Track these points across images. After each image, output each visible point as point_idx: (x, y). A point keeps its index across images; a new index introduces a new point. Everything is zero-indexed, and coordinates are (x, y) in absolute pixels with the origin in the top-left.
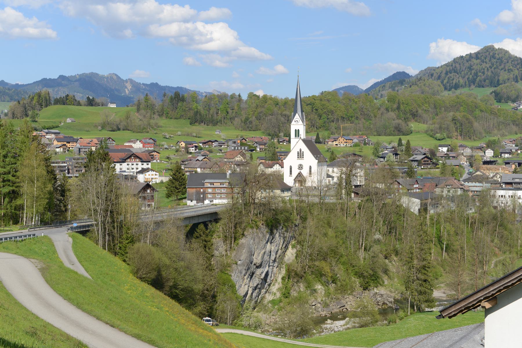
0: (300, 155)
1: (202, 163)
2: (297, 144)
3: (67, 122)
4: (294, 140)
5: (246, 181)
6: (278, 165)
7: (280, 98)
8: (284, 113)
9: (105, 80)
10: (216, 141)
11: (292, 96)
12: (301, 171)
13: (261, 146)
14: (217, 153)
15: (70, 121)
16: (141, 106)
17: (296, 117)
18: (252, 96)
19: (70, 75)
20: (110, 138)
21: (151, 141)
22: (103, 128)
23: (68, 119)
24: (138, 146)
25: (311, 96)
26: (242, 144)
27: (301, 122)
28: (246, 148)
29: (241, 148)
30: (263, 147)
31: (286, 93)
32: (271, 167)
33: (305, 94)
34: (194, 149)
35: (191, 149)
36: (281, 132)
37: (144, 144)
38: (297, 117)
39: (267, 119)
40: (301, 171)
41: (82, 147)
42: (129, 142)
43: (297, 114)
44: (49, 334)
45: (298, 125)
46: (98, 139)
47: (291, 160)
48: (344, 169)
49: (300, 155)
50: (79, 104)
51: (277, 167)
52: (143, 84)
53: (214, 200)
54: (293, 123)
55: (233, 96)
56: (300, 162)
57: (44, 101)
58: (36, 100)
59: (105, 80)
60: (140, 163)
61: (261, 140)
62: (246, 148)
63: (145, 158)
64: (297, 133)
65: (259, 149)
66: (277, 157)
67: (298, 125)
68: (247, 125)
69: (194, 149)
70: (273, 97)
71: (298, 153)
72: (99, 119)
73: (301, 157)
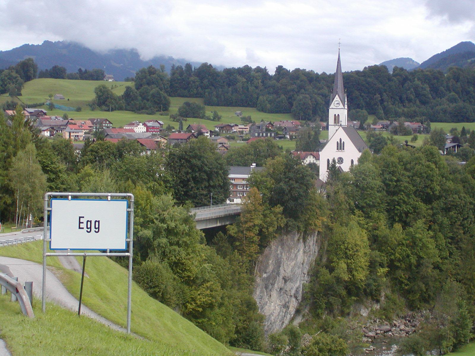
0: (340, 146)
6: (312, 157)
8: (460, 200)
11: (331, 70)
18: (280, 69)
25: (353, 70)
26: (268, 130)
27: (341, 106)
28: (273, 135)
29: (267, 135)
33: (345, 69)
34: (209, 134)
36: (320, 112)
39: (297, 95)
41: (73, 130)
43: (337, 96)
45: (338, 109)
46: (92, 120)
47: (328, 153)
49: (340, 146)
53: (235, 200)
55: (259, 69)
58: (23, 68)
62: (273, 135)
64: (337, 119)
67: (338, 109)
73: (341, 149)
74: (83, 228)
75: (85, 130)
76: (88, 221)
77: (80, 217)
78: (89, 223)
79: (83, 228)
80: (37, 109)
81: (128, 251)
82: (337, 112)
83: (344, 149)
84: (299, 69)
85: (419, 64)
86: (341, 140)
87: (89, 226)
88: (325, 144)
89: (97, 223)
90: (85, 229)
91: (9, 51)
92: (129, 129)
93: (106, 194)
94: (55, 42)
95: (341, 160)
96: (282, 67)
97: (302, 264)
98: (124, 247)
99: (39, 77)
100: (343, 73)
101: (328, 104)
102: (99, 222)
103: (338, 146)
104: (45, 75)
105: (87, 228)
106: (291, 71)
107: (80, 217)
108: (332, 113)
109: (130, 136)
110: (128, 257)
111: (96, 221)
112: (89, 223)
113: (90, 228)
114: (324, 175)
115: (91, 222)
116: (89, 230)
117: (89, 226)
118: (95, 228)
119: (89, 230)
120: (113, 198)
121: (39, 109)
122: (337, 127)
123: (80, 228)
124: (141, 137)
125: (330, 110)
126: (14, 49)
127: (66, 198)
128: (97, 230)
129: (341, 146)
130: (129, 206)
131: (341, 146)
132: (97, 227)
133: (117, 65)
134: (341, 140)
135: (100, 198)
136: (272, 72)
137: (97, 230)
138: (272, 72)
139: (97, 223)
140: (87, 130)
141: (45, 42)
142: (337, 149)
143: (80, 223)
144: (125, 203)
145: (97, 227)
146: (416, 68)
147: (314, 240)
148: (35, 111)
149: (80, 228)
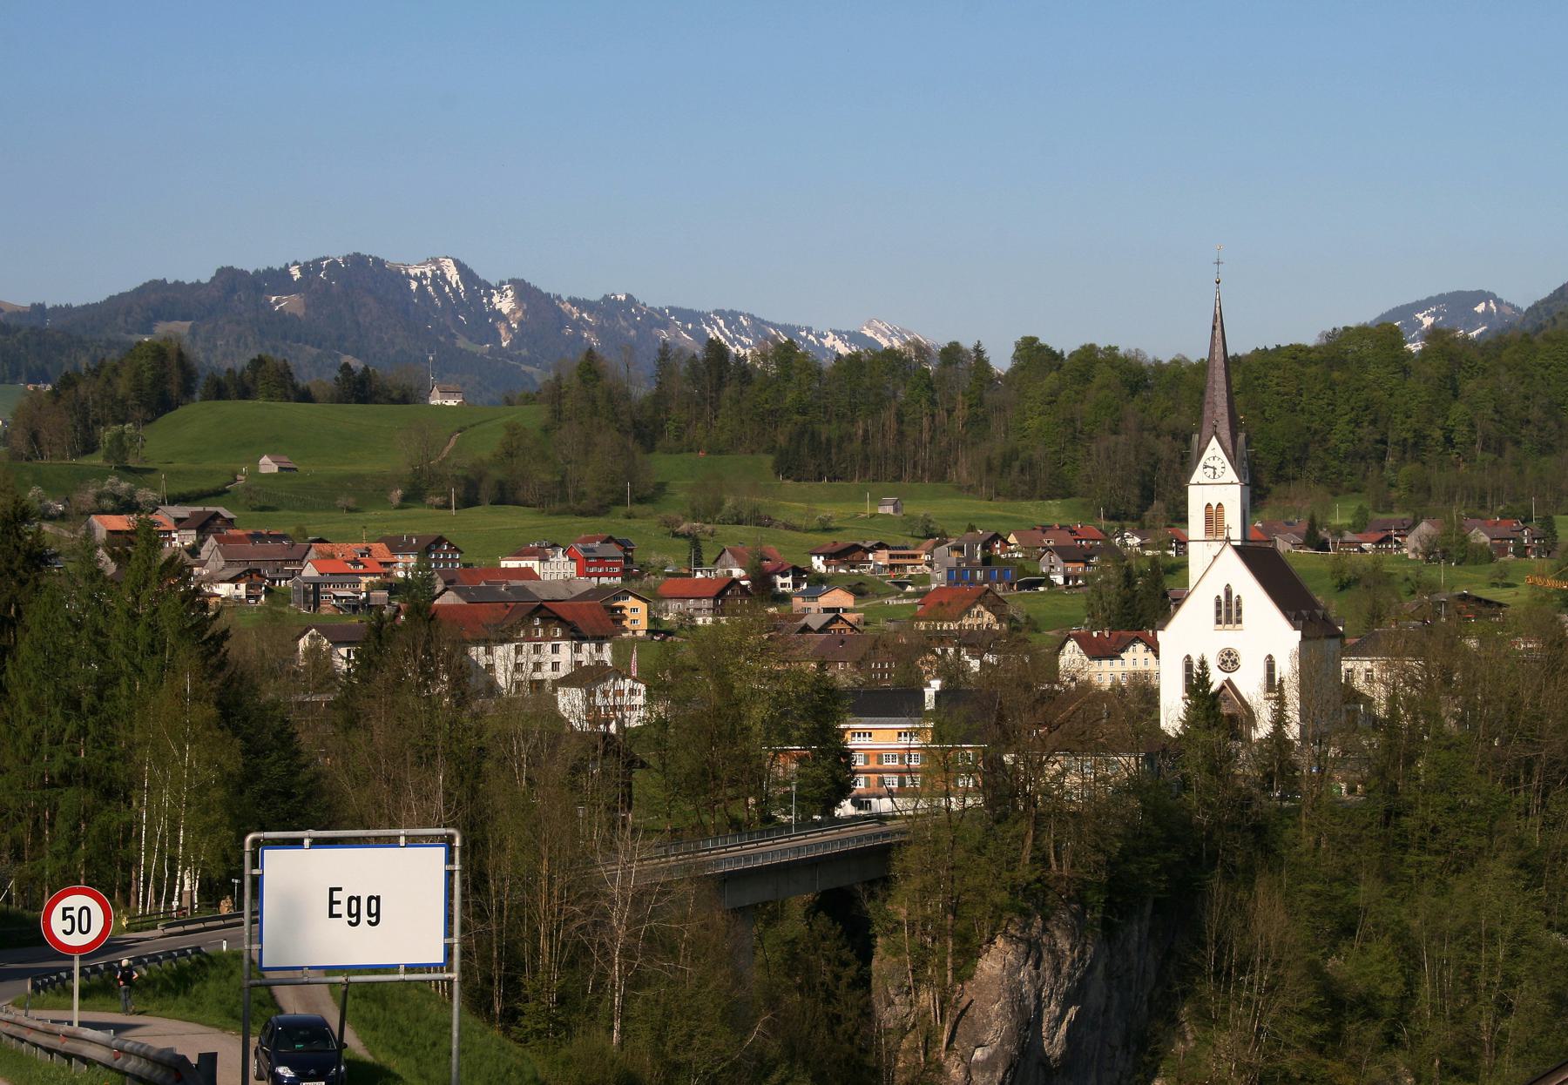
0: (1228, 611)
1: (824, 643)
2: (1215, 568)
3: (263, 470)
4: (1199, 554)
5: (1004, 714)
6: (1140, 647)
7: (1150, 358)
9: (414, 285)
10: (881, 546)
11: (1196, 349)
12: (1233, 677)
13: (1070, 567)
14: (888, 595)
15: (275, 469)
16: (567, 403)
17: (1208, 453)
18: (1032, 353)
19: (262, 267)
20: (440, 541)
21: (613, 550)
22: (414, 496)
23: (265, 459)
24: (556, 571)
30: (1080, 567)
31: (1166, 335)
32: (1114, 655)
33: (1240, 345)
34: (789, 580)
35: (780, 580)
36: (1158, 496)
37: (586, 563)
38: (1214, 452)
39: (1088, 440)
40: (1233, 677)
42: (519, 554)
44: (992, 860)
45: (1215, 485)
47: (1188, 635)
48: (1415, 664)
49: (1228, 611)
50: (305, 396)
51: (1135, 658)
52: (574, 302)
54: (1199, 475)
55: (952, 353)
56: (1228, 638)
57: (166, 383)
58: (134, 375)
59: (414, 285)
60: (565, 647)
61: (1068, 540)
63: (583, 619)
64: (1214, 517)
65: (1059, 580)
66: (1145, 602)
67: (1215, 485)
68: (1016, 476)
69: (789, 580)
70: (1121, 352)
71: (1218, 604)
72: (395, 461)
73: (1228, 621)
74: (339, 916)
75: (366, 575)
76: (351, 899)
77: (332, 890)
78: (354, 903)
79: (339, 916)
80: (200, 509)
81: (450, 970)
82: (1214, 496)
83: (1239, 622)
84: (1092, 346)
85: (1518, 310)
86: (1228, 593)
87: (354, 911)
88: (1179, 602)
89: (374, 902)
90: (346, 917)
91: (95, 305)
92: (520, 569)
93: (393, 832)
94: (257, 272)
95: (1230, 660)
96: (1034, 340)
97: (1106, 1011)
98: (439, 958)
99: (205, 398)
100: (1237, 360)
101: (1186, 462)
102: (378, 899)
103: (1218, 613)
104: (219, 391)
105: (350, 915)
106: (1066, 356)
107: (332, 890)
108: (1198, 498)
109: (523, 590)
110: (450, 981)
111: (370, 898)
112: (354, 903)
113: (358, 914)
114: (1172, 711)
115: (358, 899)
116: (354, 920)
117: (354, 911)
118: (370, 914)
119: (354, 920)
120: (413, 841)
121: (209, 509)
122: (1217, 546)
123: (332, 915)
124: (562, 594)
125: (1190, 488)
126: (111, 298)
127: (297, 843)
128: (373, 919)
129: (1229, 613)
130: (450, 860)
131: (1229, 613)
132: (374, 911)
133: (473, 347)
134: (1228, 593)
135: (379, 842)
136: (1001, 361)
137: (373, 919)
138: (1001, 361)
139: (374, 902)
140: (374, 574)
141: (222, 272)
142: (1219, 622)
143: (332, 903)
144: (441, 852)
145: (374, 911)
146: (1510, 326)
147: (180, 899)
148: (193, 514)
149: (332, 915)
